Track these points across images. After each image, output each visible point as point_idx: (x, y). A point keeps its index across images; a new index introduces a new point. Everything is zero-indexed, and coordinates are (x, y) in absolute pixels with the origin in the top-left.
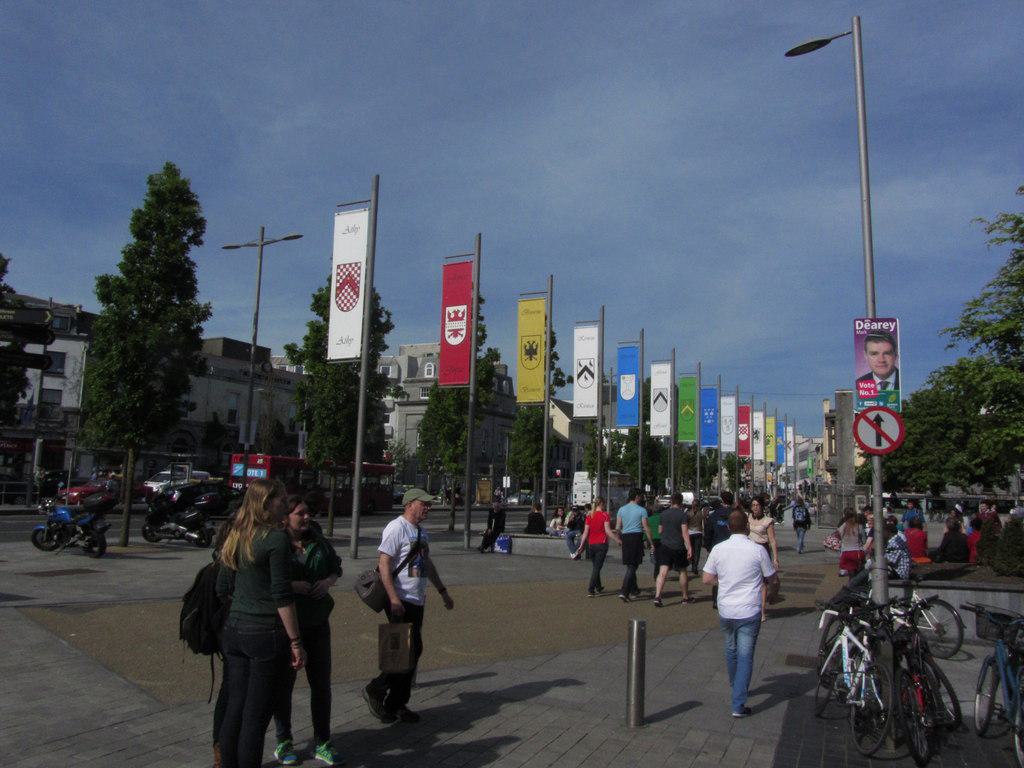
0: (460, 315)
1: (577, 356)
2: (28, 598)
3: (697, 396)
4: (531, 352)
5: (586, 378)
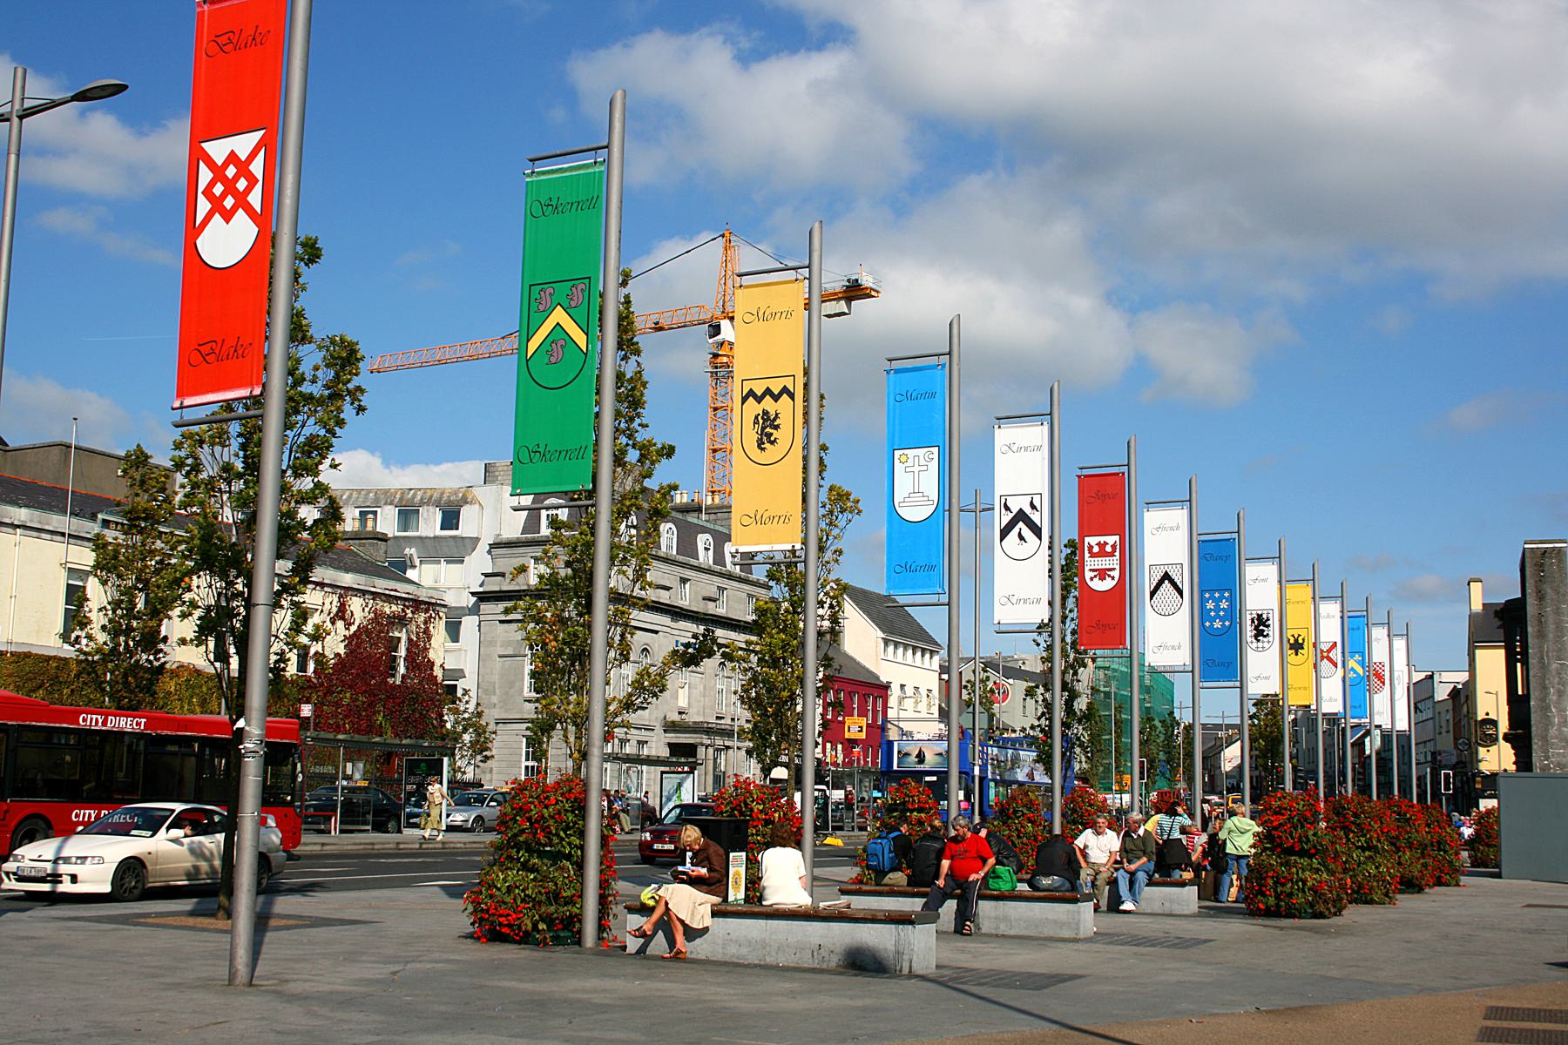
0: (1108, 549)
1: (1000, 489)
2: (99, 920)
3: (1504, 709)
4: (1261, 623)
5: (1021, 537)
